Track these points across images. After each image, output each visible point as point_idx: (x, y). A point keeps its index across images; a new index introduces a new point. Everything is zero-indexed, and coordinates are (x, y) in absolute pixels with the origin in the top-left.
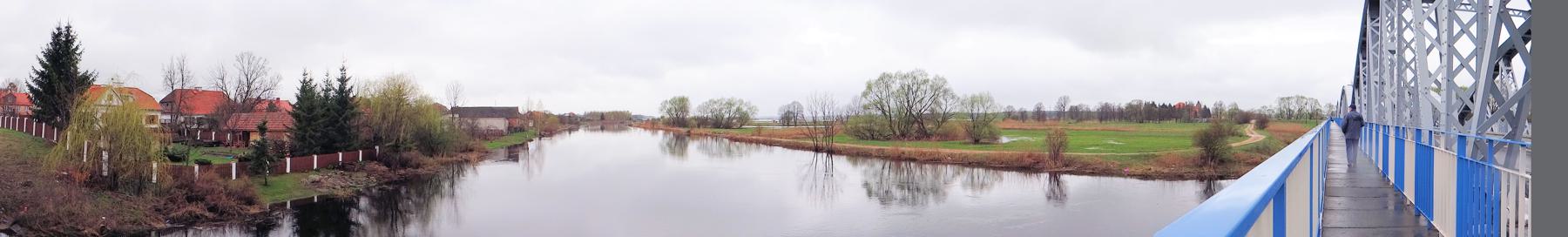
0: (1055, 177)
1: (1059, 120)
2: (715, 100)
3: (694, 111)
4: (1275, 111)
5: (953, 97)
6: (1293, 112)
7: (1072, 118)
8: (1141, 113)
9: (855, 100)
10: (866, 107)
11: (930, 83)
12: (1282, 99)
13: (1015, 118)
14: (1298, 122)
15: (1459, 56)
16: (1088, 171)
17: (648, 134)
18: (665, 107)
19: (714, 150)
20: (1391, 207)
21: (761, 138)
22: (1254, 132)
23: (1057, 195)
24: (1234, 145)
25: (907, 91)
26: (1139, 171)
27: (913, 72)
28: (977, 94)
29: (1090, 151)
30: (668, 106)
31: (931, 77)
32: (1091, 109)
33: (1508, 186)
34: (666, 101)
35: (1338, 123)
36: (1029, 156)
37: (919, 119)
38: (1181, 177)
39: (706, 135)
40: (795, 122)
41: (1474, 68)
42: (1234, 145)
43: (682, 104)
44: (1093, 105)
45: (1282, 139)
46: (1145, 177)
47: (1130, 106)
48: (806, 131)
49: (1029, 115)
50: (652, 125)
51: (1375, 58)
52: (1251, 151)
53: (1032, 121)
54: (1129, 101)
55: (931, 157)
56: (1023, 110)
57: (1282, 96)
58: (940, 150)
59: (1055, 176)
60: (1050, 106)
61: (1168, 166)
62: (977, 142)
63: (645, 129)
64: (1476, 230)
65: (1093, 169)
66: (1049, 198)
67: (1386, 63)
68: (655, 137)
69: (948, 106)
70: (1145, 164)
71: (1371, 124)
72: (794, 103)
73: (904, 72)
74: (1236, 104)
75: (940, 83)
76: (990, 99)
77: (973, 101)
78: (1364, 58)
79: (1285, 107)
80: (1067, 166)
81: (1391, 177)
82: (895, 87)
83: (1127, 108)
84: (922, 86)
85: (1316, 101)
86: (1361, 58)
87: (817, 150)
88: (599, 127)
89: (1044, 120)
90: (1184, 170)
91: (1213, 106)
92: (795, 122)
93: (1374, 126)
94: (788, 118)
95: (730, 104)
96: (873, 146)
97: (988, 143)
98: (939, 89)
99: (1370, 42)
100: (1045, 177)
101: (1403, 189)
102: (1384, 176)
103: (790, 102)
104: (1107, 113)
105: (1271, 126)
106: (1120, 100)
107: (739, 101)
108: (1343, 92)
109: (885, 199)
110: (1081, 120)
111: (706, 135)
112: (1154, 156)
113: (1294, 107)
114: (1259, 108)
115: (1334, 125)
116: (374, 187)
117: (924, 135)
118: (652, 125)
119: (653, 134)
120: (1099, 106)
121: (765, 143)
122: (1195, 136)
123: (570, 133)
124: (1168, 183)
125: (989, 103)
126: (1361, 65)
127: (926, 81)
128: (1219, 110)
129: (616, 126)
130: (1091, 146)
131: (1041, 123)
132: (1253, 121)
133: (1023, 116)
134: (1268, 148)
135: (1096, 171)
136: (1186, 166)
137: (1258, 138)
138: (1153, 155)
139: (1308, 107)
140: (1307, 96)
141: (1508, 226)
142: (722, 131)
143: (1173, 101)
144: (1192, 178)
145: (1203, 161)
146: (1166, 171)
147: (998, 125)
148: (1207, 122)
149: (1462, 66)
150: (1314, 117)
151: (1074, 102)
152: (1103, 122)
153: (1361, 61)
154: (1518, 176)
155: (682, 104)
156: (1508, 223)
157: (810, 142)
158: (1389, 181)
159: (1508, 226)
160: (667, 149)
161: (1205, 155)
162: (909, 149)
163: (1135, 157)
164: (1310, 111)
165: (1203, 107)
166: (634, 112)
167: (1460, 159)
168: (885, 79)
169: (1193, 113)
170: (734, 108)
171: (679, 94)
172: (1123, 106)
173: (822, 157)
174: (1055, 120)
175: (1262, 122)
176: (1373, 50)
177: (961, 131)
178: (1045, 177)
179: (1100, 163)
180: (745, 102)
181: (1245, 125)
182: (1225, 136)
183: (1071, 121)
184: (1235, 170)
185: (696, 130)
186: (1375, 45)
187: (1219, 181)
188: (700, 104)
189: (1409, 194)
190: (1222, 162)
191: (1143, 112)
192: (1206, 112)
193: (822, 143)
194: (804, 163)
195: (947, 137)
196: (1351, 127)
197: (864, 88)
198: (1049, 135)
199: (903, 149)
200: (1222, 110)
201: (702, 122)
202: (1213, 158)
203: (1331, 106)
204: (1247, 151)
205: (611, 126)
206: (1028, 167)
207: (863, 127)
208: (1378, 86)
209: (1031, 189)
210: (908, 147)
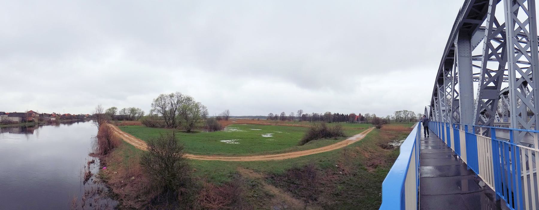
3: (118, 113)
12: (397, 112)
14: (401, 123)
41: (451, 87)
57: (396, 111)
71: (442, 123)
74: (375, 115)
81: (446, 142)
85: (413, 113)
93: (438, 123)
95: (405, 112)
101: (450, 146)
108: (426, 109)
113: (402, 115)
116: (319, 125)
123: (78, 123)
133: (276, 117)
139: (409, 116)
140: (409, 111)
143: (346, 112)
149: (448, 94)
150: (413, 120)
151: (304, 113)
158: (445, 143)
166: (41, 110)
170: (122, 111)
176: (441, 101)
182: (90, 172)
186: (442, 99)
189: (453, 147)
203: (420, 115)
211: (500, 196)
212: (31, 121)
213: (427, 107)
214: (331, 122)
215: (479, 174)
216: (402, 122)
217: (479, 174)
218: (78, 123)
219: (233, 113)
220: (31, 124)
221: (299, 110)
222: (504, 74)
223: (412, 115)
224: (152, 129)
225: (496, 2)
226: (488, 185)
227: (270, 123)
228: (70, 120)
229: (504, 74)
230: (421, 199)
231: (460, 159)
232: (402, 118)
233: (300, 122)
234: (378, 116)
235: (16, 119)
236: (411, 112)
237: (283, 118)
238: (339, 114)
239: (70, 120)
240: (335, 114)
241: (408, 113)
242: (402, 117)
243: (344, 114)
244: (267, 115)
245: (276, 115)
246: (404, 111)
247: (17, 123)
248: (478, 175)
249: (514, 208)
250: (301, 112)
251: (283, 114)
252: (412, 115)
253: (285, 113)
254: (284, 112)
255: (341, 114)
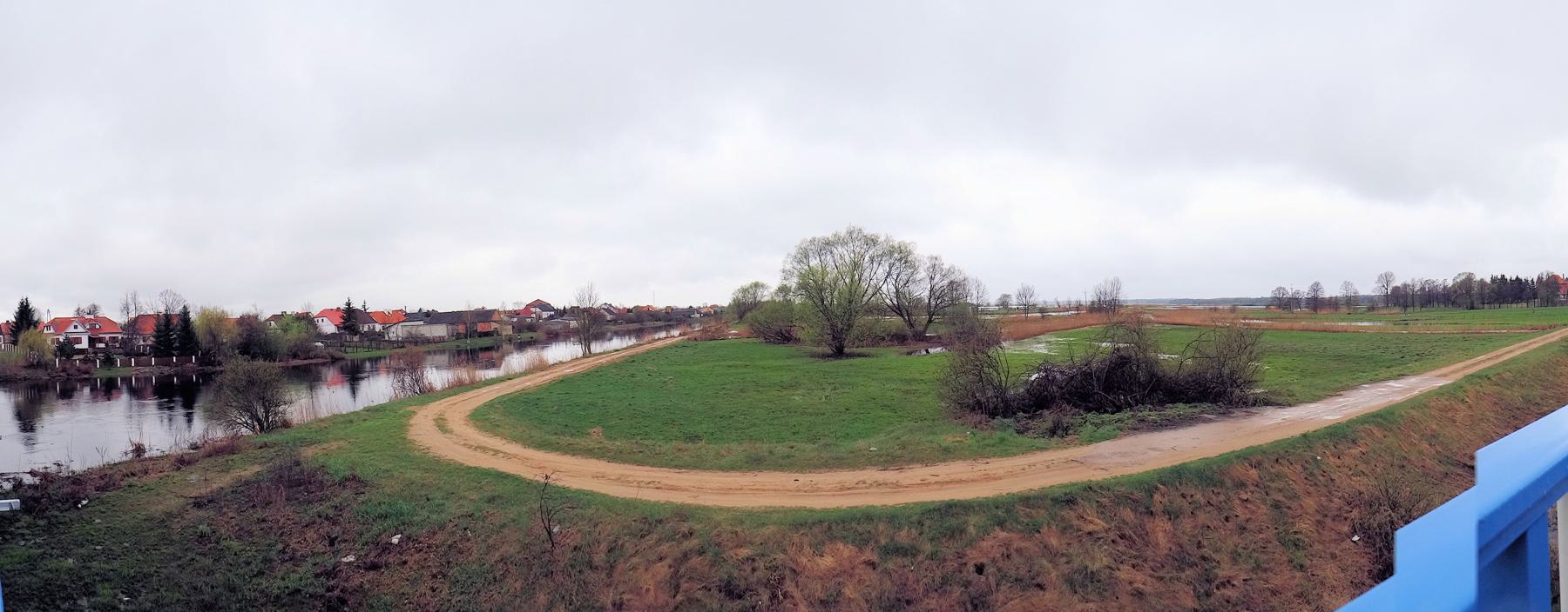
143: (1529, 272)
151: (1398, 282)
212: (487, 334)
214: (1476, 305)
219: (1046, 295)
220: (486, 342)
221: (1383, 272)
224: (783, 349)
227: (1267, 319)
228: (636, 326)
233: (1396, 310)
234: (1133, 293)
235: (440, 331)
237: (1316, 303)
238: (1508, 277)
239: (636, 326)
240: (1494, 280)
243: (1522, 277)
244: (1267, 293)
245: (1482, 280)
247: (441, 340)
250: (1387, 278)
251: (1316, 287)
255: (1514, 278)
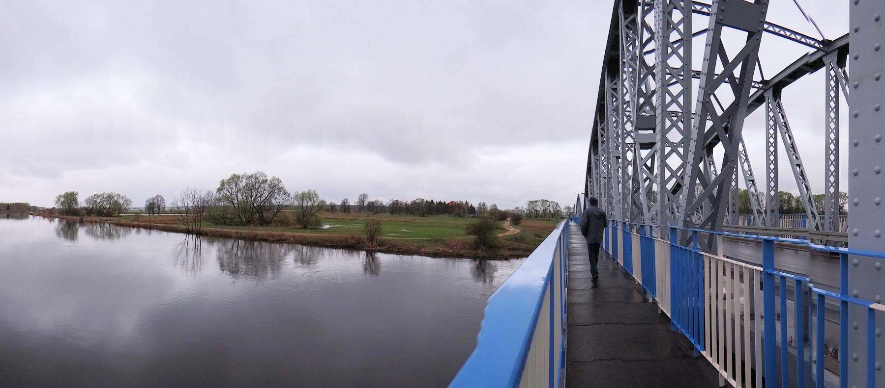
0: (371, 254)
1: (360, 212)
2: (99, 194)
3: (82, 202)
4: (525, 211)
5: (285, 193)
6: (539, 211)
7: (370, 211)
8: (422, 209)
9: (208, 194)
10: (219, 200)
11: (269, 182)
12: (531, 202)
13: (327, 210)
14: (544, 220)
15: (670, 169)
16: (395, 250)
17: (46, 221)
18: (59, 200)
19: (99, 234)
20: (604, 258)
21: (142, 224)
22: (510, 227)
23: (372, 267)
24: (499, 235)
25: (250, 188)
26: (432, 251)
27: (256, 174)
28: (306, 191)
29: (391, 236)
30: (62, 199)
31: (269, 178)
32: (384, 204)
33: (710, 267)
34: (60, 196)
35: (575, 221)
36: (353, 238)
37: (261, 209)
38: (461, 256)
39: (96, 222)
40: (159, 212)
42: (499, 235)
43: (71, 198)
44: (386, 201)
45: (533, 232)
46: (435, 255)
47: (414, 203)
48: (180, 218)
49: (338, 208)
50: (49, 214)
51: (596, 178)
52: (511, 240)
53: (340, 213)
54: (414, 199)
55: (279, 238)
56: (333, 204)
58: (285, 233)
59: (370, 254)
60: (353, 202)
61: (452, 248)
62: (305, 228)
63: (44, 217)
64: (686, 304)
65: (398, 249)
66: (366, 269)
67: (602, 183)
68: (52, 223)
69: (278, 200)
70: (435, 246)
72: (157, 196)
73: (249, 174)
74: (495, 205)
75: (276, 182)
76: (315, 195)
77: (303, 196)
78: (591, 178)
79: (533, 208)
80: (380, 246)
81: (621, 261)
82: (242, 184)
83: (412, 204)
84: (262, 185)
86: (588, 178)
87: (188, 232)
88: (5, 215)
89: (349, 212)
90: (463, 251)
91: (478, 205)
92: (159, 212)
94: (153, 207)
96: (233, 230)
97: (314, 229)
98: (276, 187)
99: (594, 169)
100: (363, 254)
102: (614, 260)
103: (155, 196)
104: (397, 208)
105: (523, 223)
106: (407, 198)
107: (117, 195)
108: (578, 199)
109: (234, 271)
110: (377, 213)
111: (96, 222)
112: (441, 240)
113: (540, 208)
114: (513, 208)
115: (572, 223)
117: (264, 222)
118: (49, 214)
119: (51, 221)
120: (390, 202)
121: (145, 227)
122: (468, 228)
123: (44, 218)
124: (450, 261)
125: (315, 199)
126: (589, 182)
127: (265, 181)
128: (482, 207)
129: (18, 215)
130: (391, 233)
131: (347, 214)
132: (509, 219)
134: (523, 238)
135: (401, 250)
136: (465, 248)
137: (515, 231)
138: (441, 239)
139: (551, 208)
141: (710, 299)
142: (104, 218)
143: (447, 199)
144: (468, 257)
145: (476, 246)
146: (450, 251)
147: (322, 215)
148: (473, 217)
150: (555, 216)
152: (394, 215)
153: (589, 180)
154: (717, 259)
155: (71, 198)
156: (710, 297)
157: (183, 227)
158: (618, 263)
159: (710, 299)
160: (62, 233)
161: (478, 241)
162: (261, 232)
163: (429, 241)
164: (552, 212)
165: (470, 205)
167: (672, 246)
168: (235, 179)
169: (462, 210)
171: (70, 190)
172: (409, 202)
173: (192, 238)
174: (357, 212)
175: (516, 218)
176: (602, 150)
177: (292, 218)
178: (363, 254)
179: (404, 245)
180: (121, 196)
181: (503, 221)
183: (369, 213)
184: (501, 254)
185: (86, 218)
186: (603, 125)
187: (488, 261)
188: (87, 197)
190: (491, 247)
191: (424, 208)
192: (472, 210)
193: (192, 227)
194: (178, 243)
195: (284, 223)
196: (592, 228)
197: (218, 186)
198: (367, 223)
199: (258, 232)
200: (485, 209)
201: (89, 212)
202: (485, 244)
203: (569, 208)
204: (508, 240)
205: (15, 215)
206: (350, 246)
207: (218, 215)
208: (598, 195)
209: (355, 262)
210: (261, 231)
211: (693, 343)
213: (580, 194)
215: (656, 297)
216: (539, 218)
217: (656, 297)
218: (44, 218)
222: (753, 80)
223: (554, 207)
225: (667, 39)
226: (707, 357)
229: (753, 80)
230: (568, 365)
231: (655, 303)
232: (539, 211)
236: (554, 202)
241: (548, 204)
242: (539, 209)
246: (543, 200)
248: (704, 353)
249: (735, 380)
252: (554, 207)
253: (349, 200)
254: (348, 198)
255: (438, 202)
